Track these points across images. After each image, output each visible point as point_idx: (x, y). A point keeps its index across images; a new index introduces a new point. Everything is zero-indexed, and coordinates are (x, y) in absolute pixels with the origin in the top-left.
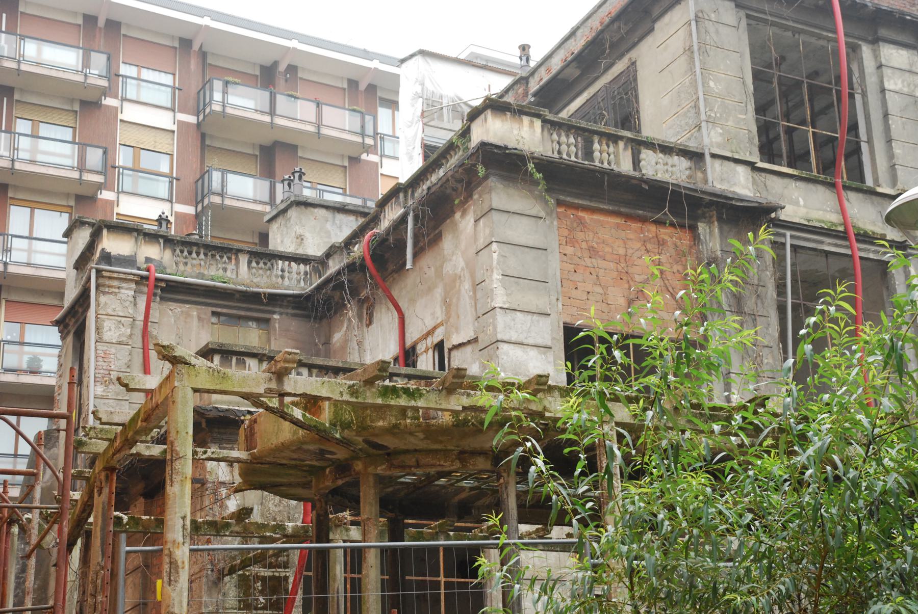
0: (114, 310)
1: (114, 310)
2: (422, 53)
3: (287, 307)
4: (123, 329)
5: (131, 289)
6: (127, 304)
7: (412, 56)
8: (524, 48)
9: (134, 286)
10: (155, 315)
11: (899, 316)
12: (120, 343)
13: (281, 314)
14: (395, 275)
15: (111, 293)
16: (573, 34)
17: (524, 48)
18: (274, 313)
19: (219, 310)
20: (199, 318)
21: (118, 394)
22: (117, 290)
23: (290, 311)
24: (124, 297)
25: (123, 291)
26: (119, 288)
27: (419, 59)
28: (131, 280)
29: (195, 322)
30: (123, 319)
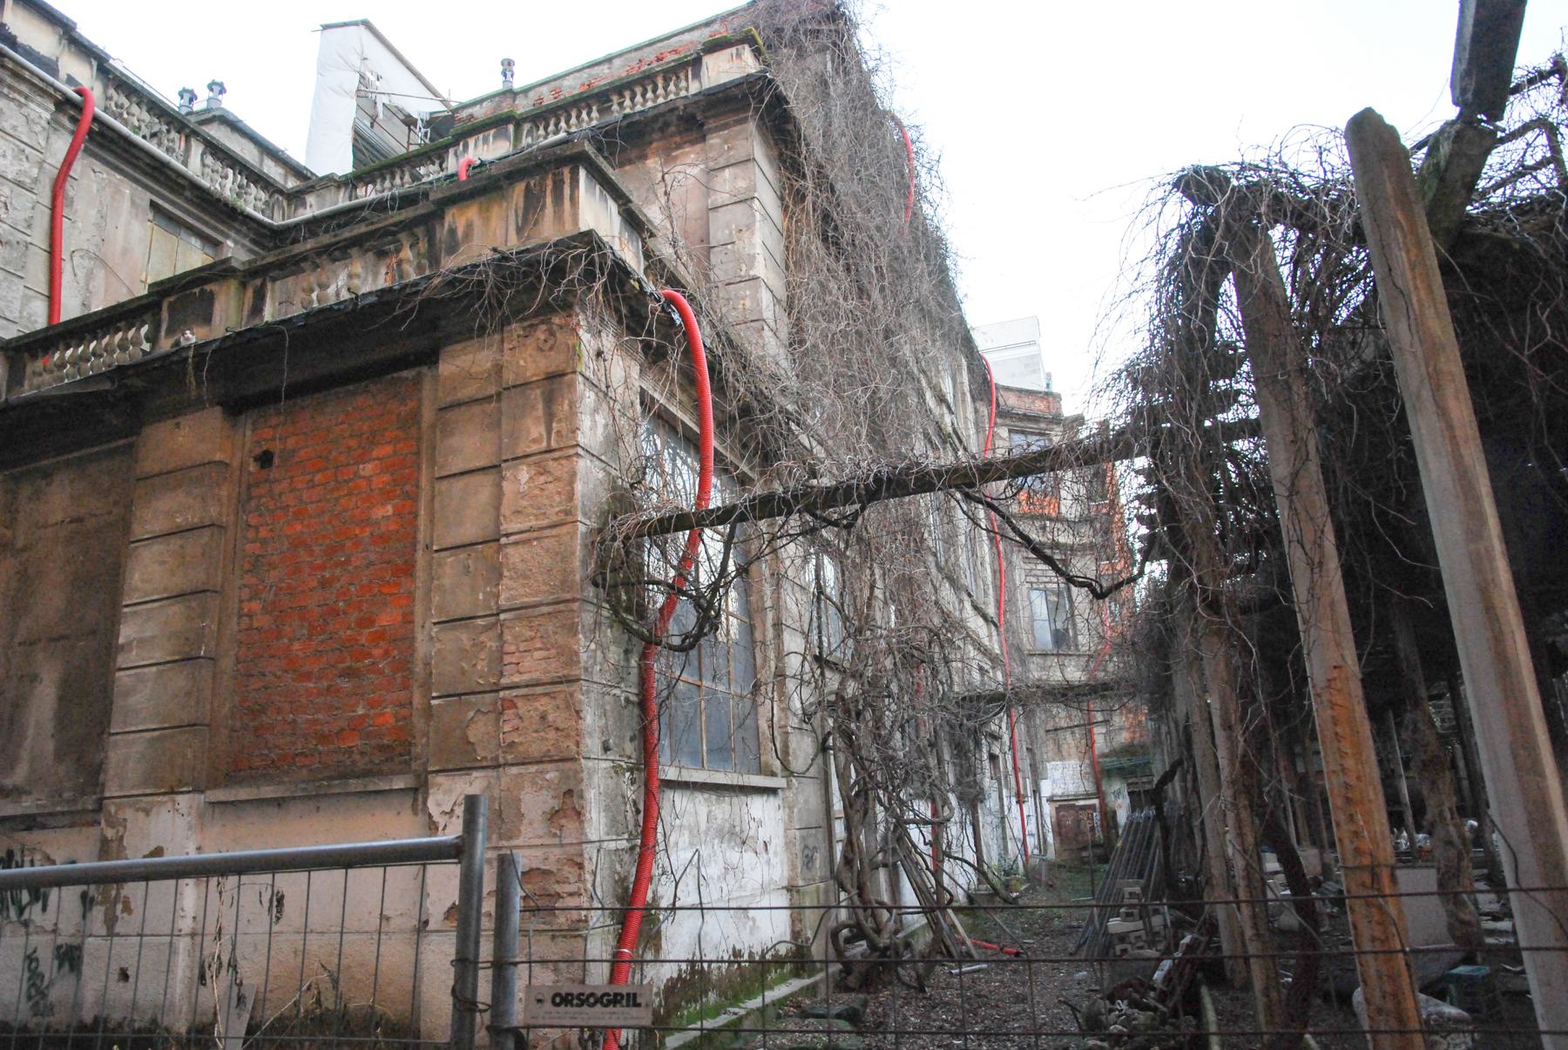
0: (15, 128)
1: (15, 128)
2: (366, 24)
3: (246, 236)
4: (26, 165)
5: (46, 109)
6: (37, 129)
7: (356, 24)
8: (508, 65)
9: (52, 108)
10: (77, 169)
11: (1235, 350)
12: (19, 184)
13: (236, 242)
14: (776, 153)
15: (13, 100)
16: (609, 60)
17: (508, 65)
18: (228, 237)
19: (160, 202)
20: (133, 202)
21: (7, 263)
22: (22, 100)
23: (247, 242)
24: (33, 116)
25: (32, 105)
26: (26, 97)
27: (362, 28)
28: (50, 95)
29: (126, 205)
30: (28, 150)
